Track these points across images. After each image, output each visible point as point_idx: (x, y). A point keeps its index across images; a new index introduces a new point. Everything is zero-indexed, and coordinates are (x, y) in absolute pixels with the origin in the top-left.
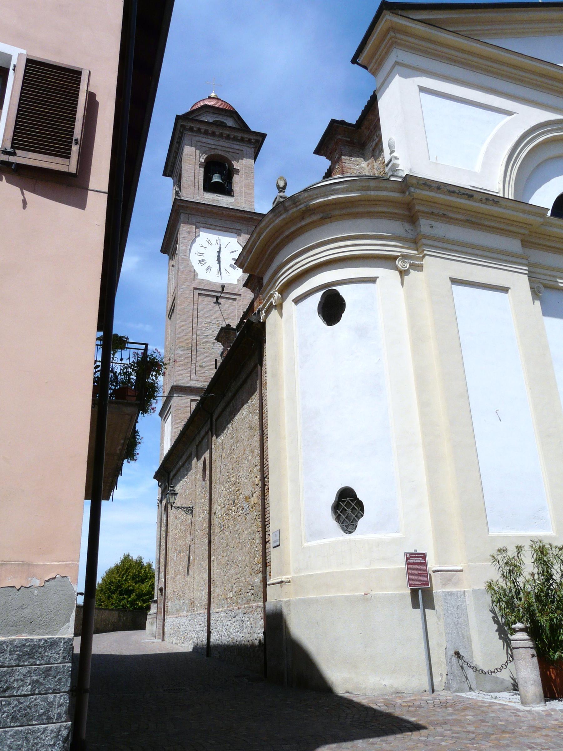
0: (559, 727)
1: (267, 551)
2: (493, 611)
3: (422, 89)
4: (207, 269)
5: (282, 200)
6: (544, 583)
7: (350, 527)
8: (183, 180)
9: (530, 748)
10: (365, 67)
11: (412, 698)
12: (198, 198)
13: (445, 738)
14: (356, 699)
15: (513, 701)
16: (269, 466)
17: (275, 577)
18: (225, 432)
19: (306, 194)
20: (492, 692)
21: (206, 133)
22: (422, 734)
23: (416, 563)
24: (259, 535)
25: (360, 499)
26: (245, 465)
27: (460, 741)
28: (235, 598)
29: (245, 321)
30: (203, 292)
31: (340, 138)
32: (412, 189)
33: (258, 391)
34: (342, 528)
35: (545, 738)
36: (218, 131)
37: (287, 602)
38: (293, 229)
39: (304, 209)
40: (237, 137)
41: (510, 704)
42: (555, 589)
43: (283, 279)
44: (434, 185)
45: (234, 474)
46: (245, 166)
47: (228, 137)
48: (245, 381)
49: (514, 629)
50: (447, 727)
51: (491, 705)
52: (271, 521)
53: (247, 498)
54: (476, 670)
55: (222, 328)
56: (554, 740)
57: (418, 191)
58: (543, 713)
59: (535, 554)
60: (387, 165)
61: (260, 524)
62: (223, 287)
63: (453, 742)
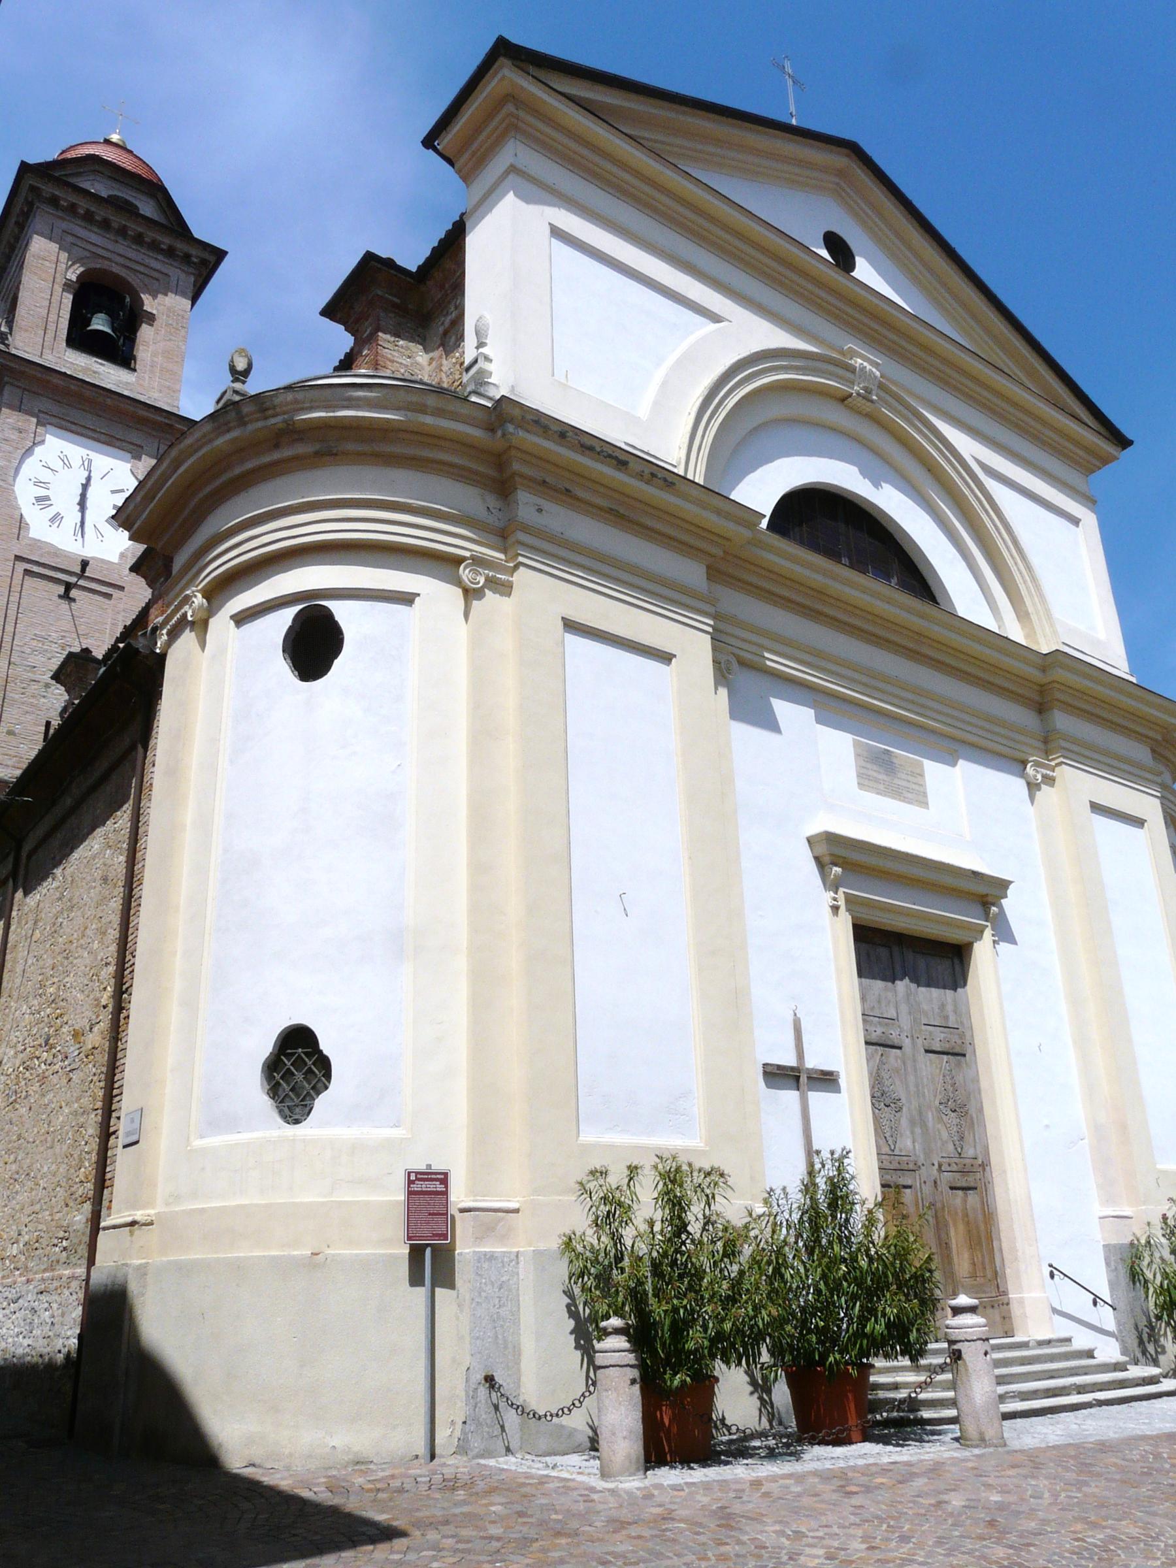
0: (664, 1519)
1: (109, 1153)
2: (569, 1294)
3: (557, 233)
4: (52, 520)
5: (237, 398)
6: (670, 1240)
7: (297, 1110)
8: (21, 311)
9: (604, 1563)
10: (451, 162)
11: (387, 1474)
12: (50, 357)
13: (441, 1554)
14: (267, 1480)
15: (587, 1471)
16: (136, 967)
17: (119, 1211)
18: (45, 884)
19: (290, 396)
20: (549, 1454)
21: (88, 217)
22: (396, 1548)
23: (427, 1192)
24: (94, 1119)
25: (325, 1052)
26: (83, 961)
27: (469, 1557)
28: (23, 1258)
29: (121, 645)
30: (35, 569)
31: (379, 293)
32: (510, 428)
33: (131, 802)
34: (281, 1112)
35: (635, 1542)
36: (117, 220)
37: (139, 1268)
38: (249, 465)
39: (281, 426)
40: (161, 242)
41: (580, 1478)
42: (688, 1251)
43: (219, 564)
44: (554, 428)
45: (56, 980)
46: (169, 309)
47: (138, 240)
48: (105, 778)
49: (605, 1329)
50: (449, 1530)
51: (543, 1481)
52: (125, 1089)
53: (77, 1035)
54: (523, 1412)
55: (71, 655)
56: (650, 1545)
57: (521, 433)
58: (638, 1493)
59: (661, 1184)
60: (468, 369)
61: (101, 1093)
62: (85, 564)
63: (455, 1560)
